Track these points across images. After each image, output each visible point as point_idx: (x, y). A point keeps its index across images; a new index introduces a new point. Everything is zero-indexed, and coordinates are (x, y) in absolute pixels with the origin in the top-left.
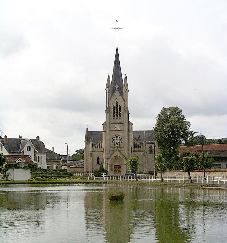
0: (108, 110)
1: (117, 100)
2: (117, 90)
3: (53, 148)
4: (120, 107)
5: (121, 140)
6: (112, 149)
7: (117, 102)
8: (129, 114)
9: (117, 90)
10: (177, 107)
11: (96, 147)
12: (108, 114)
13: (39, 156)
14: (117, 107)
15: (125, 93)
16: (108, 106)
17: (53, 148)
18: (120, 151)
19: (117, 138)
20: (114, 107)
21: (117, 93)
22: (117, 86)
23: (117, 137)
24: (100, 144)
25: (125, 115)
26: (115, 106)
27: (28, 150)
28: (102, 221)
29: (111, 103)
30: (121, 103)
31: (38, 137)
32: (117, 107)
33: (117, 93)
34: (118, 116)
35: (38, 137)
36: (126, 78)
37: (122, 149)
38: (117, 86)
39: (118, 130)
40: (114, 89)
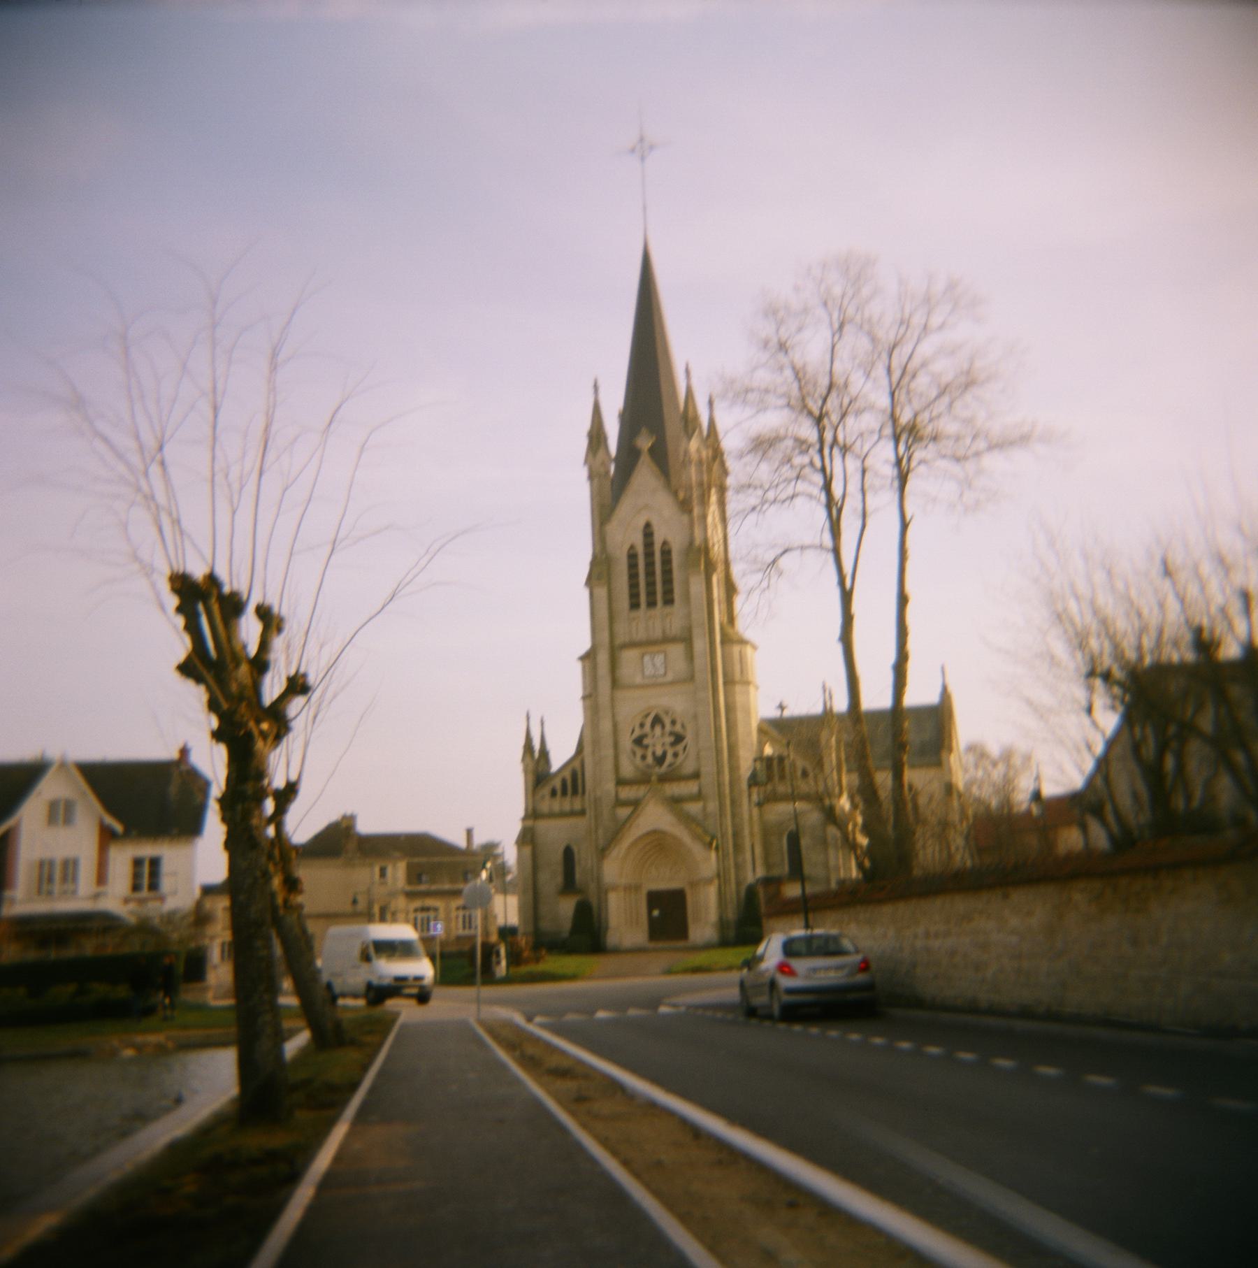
0: (600, 572)
2: (645, 459)
4: (667, 553)
5: (678, 739)
6: (627, 793)
7: (648, 525)
8: (738, 602)
9: (645, 459)
10: (212, 579)
11: (554, 793)
12: (602, 592)
14: (649, 554)
16: (714, 498)
18: (675, 802)
19: (658, 730)
20: (632, 556)
21: (645, 475)
22: (645, 442)
23: (657, 720)
26: (640, 550)
29: (613, 528)
30: (670, 530)
31: (184, 752)
32: (649, 554)
33: (645, 475)
35: (184, 752)
37: (690, 788)
39: (661, 680)
40: (628, 457)
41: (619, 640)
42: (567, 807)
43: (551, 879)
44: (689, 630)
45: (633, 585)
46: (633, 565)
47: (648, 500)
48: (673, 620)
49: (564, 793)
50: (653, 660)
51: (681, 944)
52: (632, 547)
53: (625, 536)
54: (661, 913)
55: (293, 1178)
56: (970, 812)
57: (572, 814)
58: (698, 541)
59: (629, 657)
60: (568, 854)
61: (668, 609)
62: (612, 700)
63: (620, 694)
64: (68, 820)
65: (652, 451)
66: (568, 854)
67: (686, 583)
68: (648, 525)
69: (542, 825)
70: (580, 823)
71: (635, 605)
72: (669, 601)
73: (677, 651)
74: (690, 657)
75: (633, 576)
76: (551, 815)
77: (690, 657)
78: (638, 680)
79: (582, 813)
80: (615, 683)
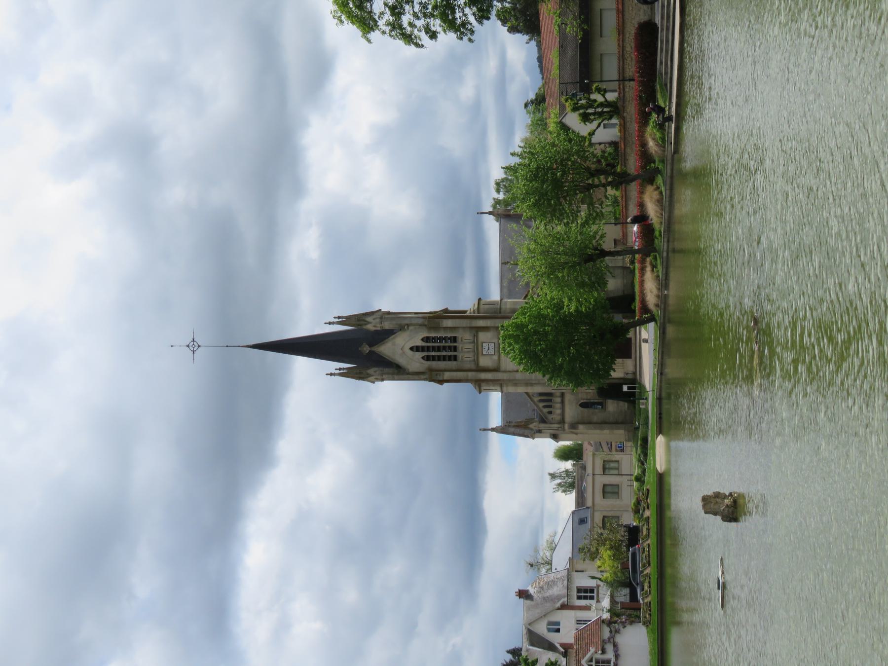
1: (407, 349)
3: (369, 41)
7: (412, 349)
12: (447, 375)
13: (575, 590)
14: (428, 349)
15: (387, 326)
17: (369, 41)
20: (427, 358)
21: (387, 349)
22: (366, 349)
24: (541, 401)
25: (449, 323)
26: (425, 354)
27: (558, 631)
28: (762, 289)
32: (428, 349)
33: (387, 349)
34: (455, 353)
36: (339, 317)
38: (366, 349)
41: (473, 366)
42: (559, 406)
43: (597, 414)
44: (471, 328)
45: (444, 358)
46: (433, 358)
47: (398, 348)
48: (465, 337)
49: (550, 406)
50: (641, 193)
51: (633, 341)
52: (423, 358)
53: (416, 362)
54: (622, 388)
55: (633, 299)
56: (730, 437)
57: (563, 402)
58: (421, 321)
59: (484, 362)
60: (584, 405)
61: (459, 340)
62: (505, 372)
63: (503, 367)
64: (558, 624)
65: (371, 345)
66: (584, 405)
67: (446, 328)
68: (412, 349)
69: (568, 418)
70: (568, 397)
71: (455, 358)
72: (454, 339)
73: (482, 336)
74: (485, 329)
75: (439, 358)
76: (563, 414)
77: (485, 329)
78: (496, 357)
79: (563, 395)
80: (496, 370)
